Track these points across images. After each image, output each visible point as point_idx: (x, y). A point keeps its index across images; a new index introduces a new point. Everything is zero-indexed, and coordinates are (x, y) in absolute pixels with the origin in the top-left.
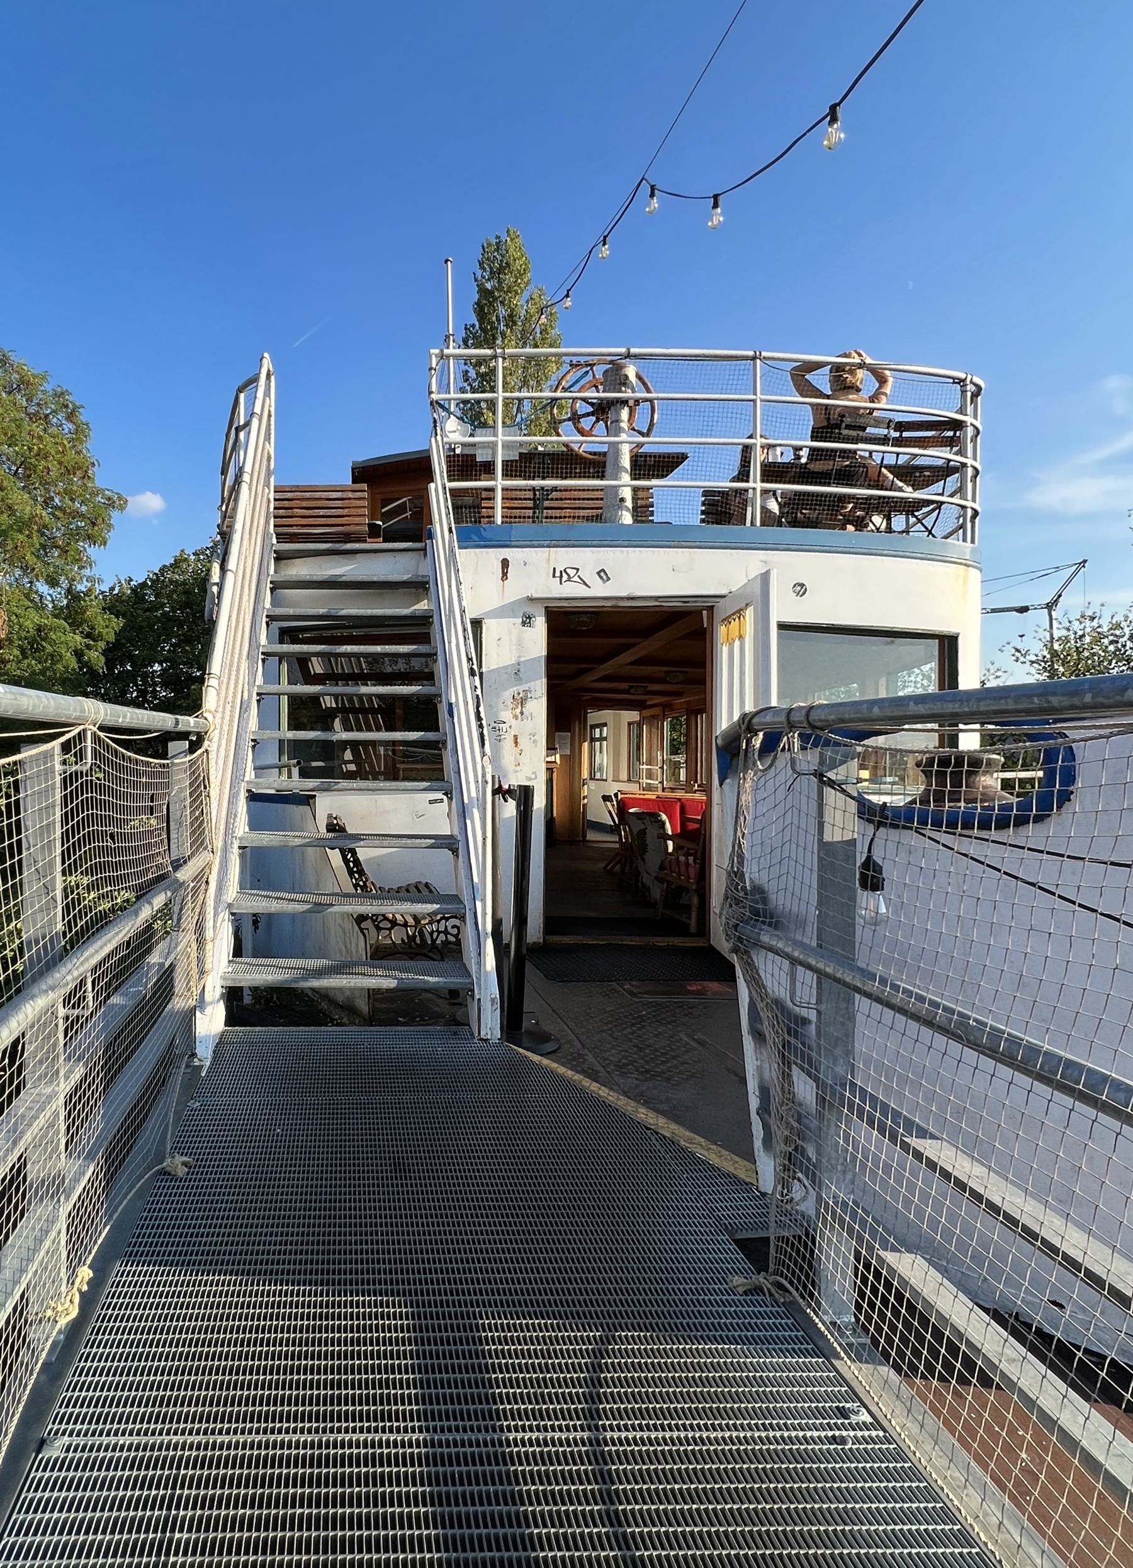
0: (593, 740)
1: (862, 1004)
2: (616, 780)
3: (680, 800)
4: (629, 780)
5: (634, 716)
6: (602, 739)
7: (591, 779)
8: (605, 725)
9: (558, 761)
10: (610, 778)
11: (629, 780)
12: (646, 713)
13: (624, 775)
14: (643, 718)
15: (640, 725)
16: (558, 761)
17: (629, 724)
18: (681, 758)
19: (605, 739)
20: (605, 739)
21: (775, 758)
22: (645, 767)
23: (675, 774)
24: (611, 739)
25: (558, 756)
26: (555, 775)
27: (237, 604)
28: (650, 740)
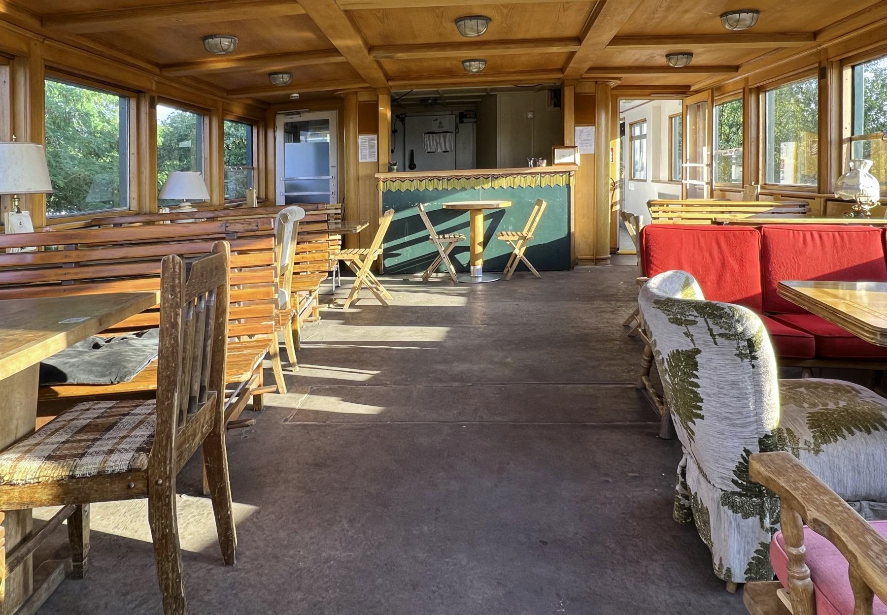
0: (632, 138)
1: (812, 84)
2: (656, 180)
3: (759, 227)
4: (671, 180)
5: (673, 106)
6: (642, 137)
7: (631, 179)
8: (645, 121)
9: (578, 162)
10: (650, 178)
11: (671, 180)
12: (690, 101)
13: (664, 175)
14: (686, 108)
15: (683, 116)
16: (578, 162)
17: (671, 118)
18: (734, 152)
19: (645, 136)
20: (645, 136)
21: (693, 456)
22: (688, 165)
23: (726, 173)
24: (650, 137)
25: (578, 156)
26: (572, 178)
27: (761, 146)
28: (695, 132)
